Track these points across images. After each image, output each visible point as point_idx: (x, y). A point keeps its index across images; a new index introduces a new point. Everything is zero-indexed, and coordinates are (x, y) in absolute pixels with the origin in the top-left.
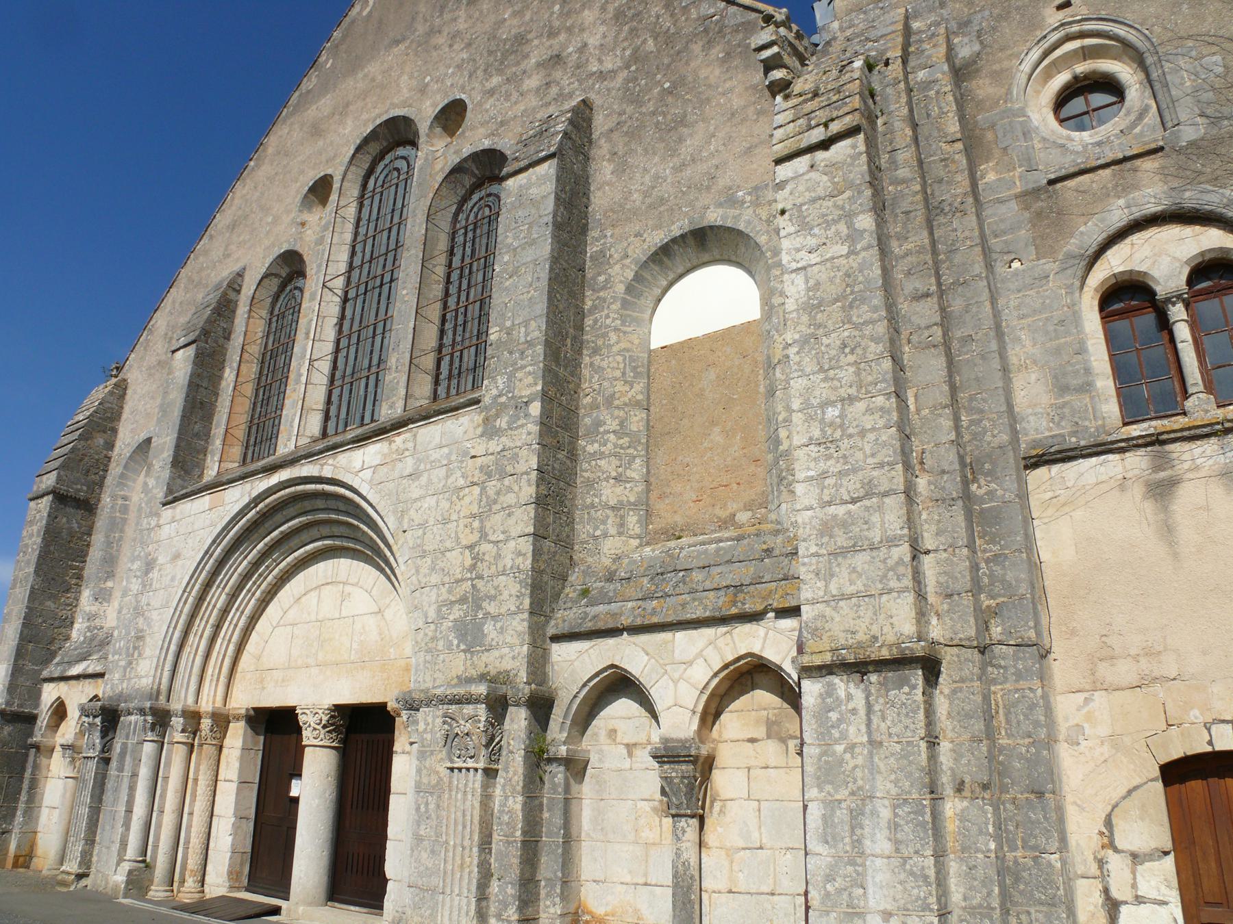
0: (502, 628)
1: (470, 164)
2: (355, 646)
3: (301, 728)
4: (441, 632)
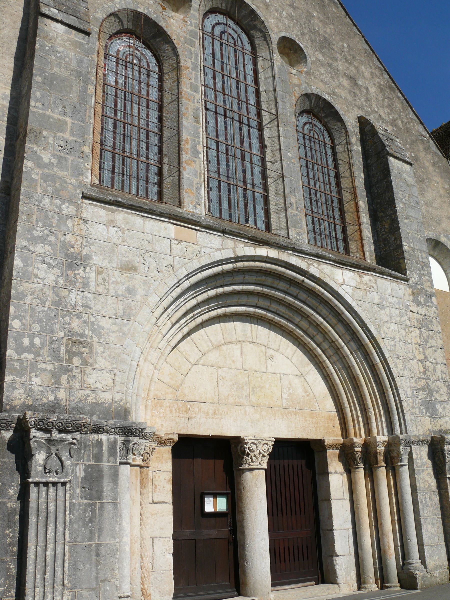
0: (444, 408)
1: (313, 99)
2: (285, 396)
3: (269, 455)
4: (416, 405)
